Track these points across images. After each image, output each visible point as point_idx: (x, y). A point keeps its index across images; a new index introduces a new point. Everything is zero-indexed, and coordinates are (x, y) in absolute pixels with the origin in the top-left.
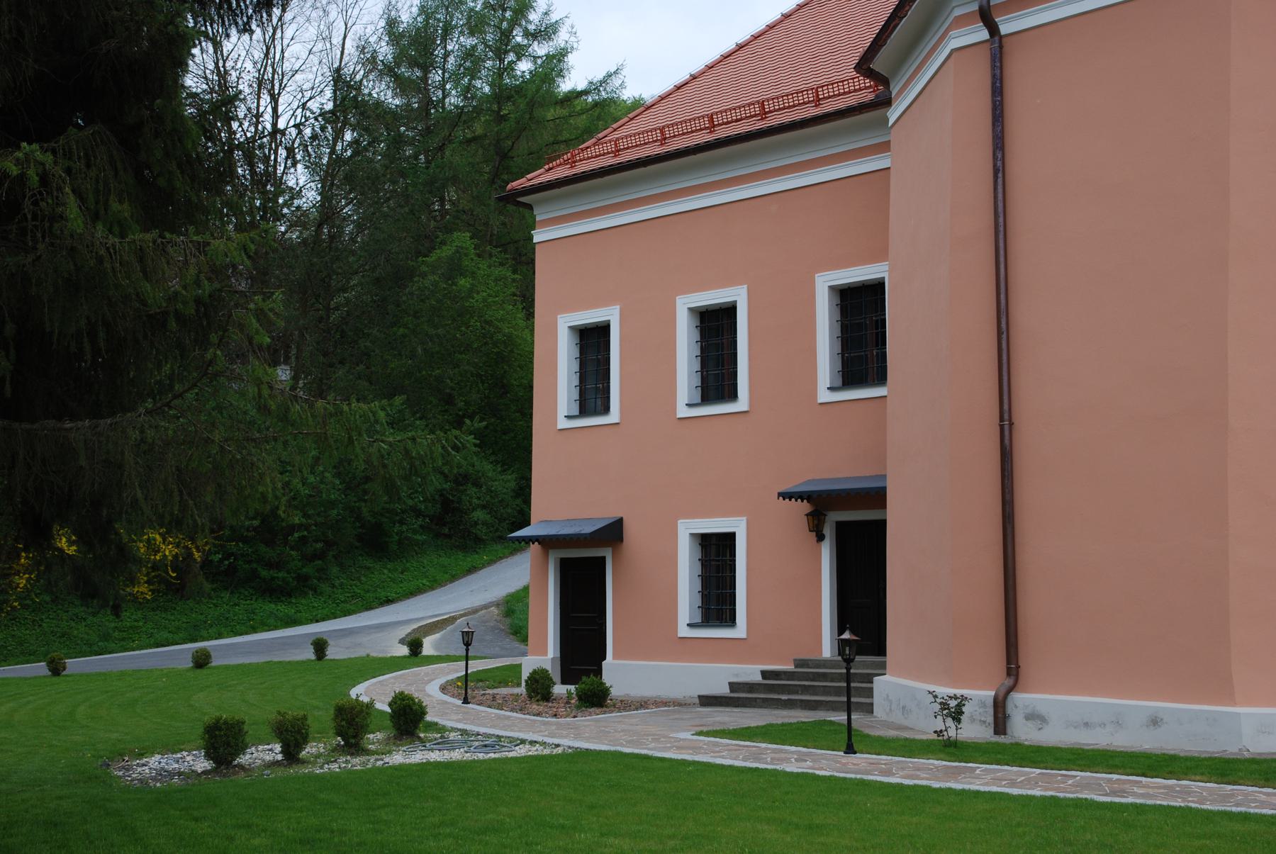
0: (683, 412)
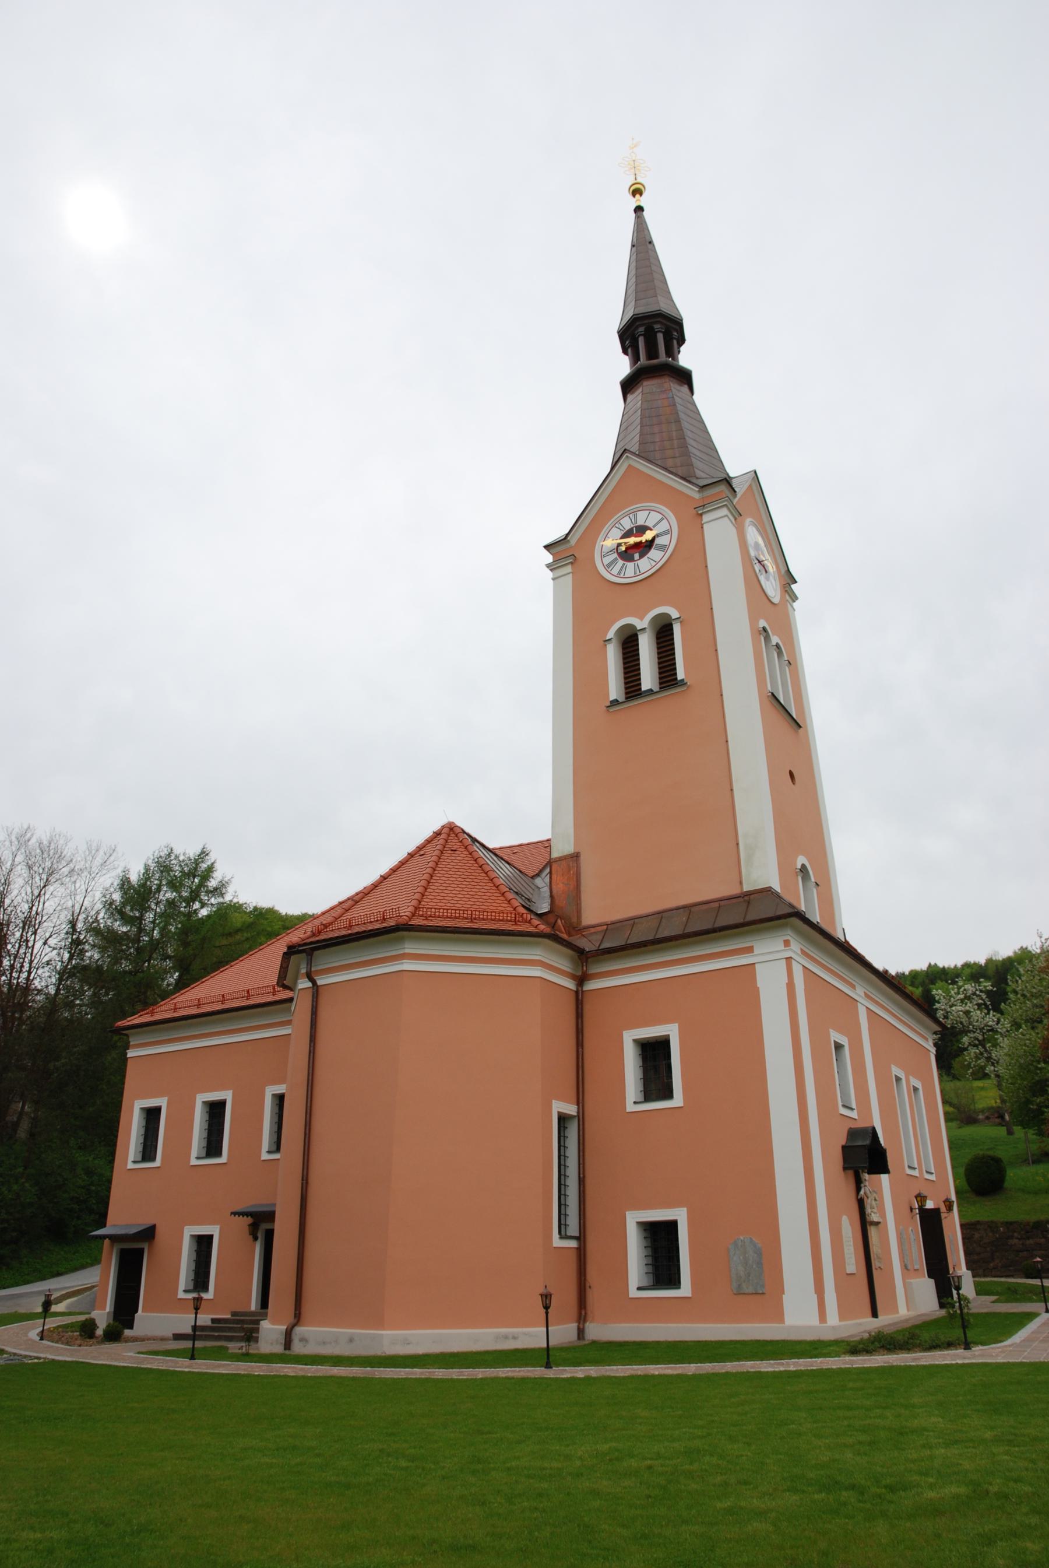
0: (194, 1162)
